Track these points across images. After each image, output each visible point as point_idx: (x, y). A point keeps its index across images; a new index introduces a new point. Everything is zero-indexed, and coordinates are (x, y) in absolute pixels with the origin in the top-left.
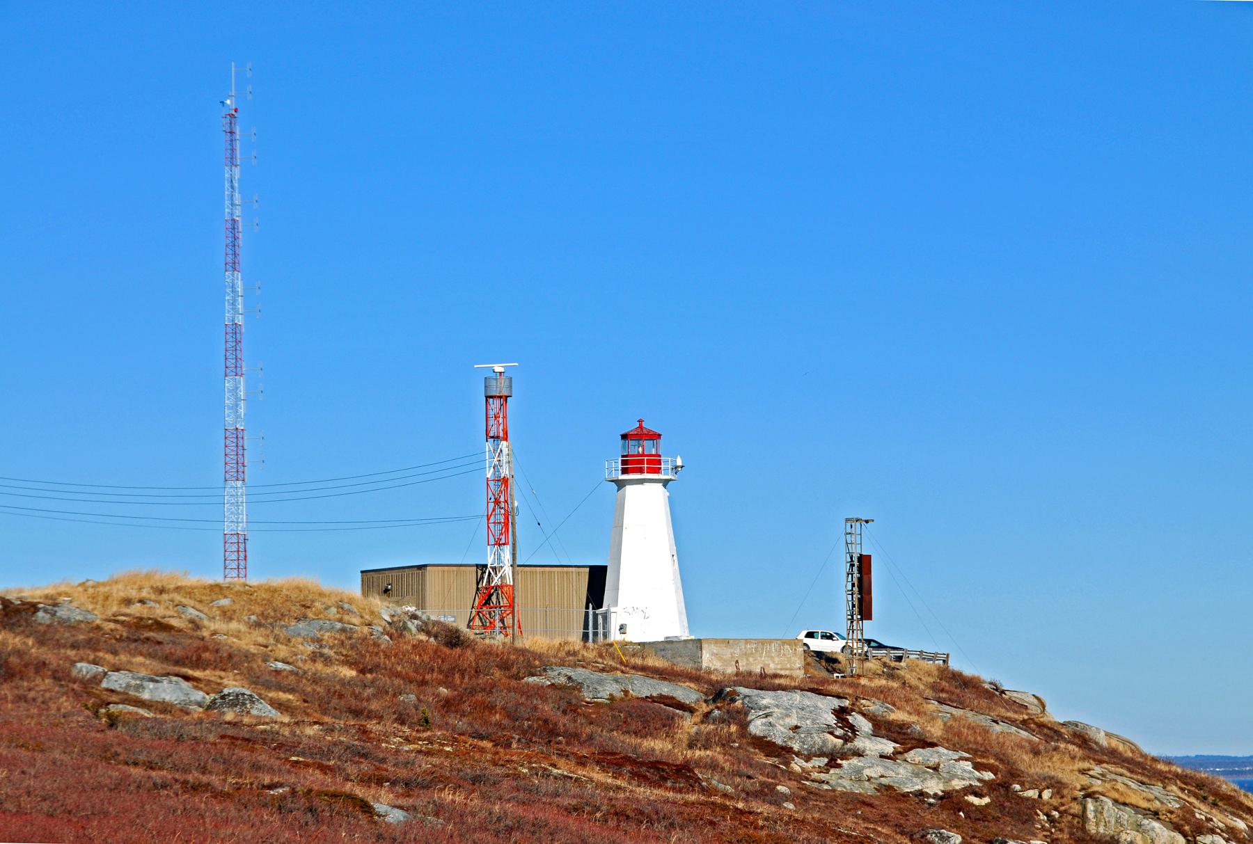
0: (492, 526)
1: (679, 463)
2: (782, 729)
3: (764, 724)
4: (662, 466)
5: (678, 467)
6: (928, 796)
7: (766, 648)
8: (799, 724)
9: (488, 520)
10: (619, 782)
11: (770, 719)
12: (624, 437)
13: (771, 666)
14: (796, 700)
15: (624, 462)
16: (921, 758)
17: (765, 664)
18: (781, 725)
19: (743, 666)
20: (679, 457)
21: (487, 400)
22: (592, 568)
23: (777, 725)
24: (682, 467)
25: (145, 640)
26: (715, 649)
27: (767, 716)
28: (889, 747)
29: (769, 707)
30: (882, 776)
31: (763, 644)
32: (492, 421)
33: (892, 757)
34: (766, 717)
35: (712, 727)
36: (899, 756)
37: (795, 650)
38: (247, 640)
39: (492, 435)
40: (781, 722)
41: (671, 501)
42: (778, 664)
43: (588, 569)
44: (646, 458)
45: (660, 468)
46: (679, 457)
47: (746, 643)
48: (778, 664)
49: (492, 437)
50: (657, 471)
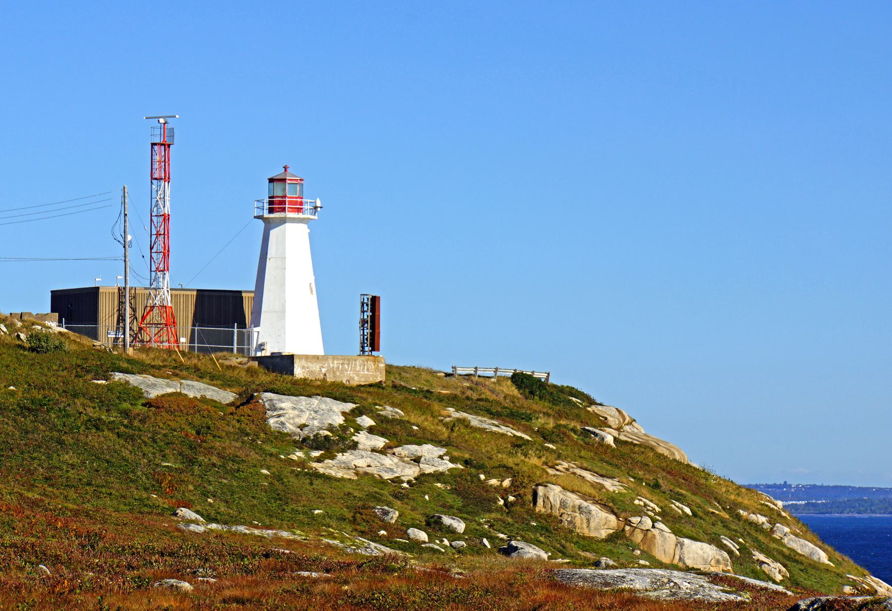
0: (154, 255)
1: (319, 204)
2: (291, 427)
3: (277, 422)
4: (287, 206)
5: (318, 207)
6: (403, 482)
7: (352, 364)
8: (307, 424)
9: (151, 248)
10: (656, 594)
11: (282, 419)
12: (271, 180)
13: (355, 378)
14: (313, 404)
15: (271, 203)
16: (406, 452)
17: (351, 377)
18: (290, 424)
19: (330, 378)
20: (318, 199)
21: (152, 148)
22: (198, 291)
23: (286, 423)
24: (321, 207)
25: (322, 459)
26: (303, 362)
27: (279, 416)
28: (380, 442)
29: (284, 409)
30: (369, 466)
31: (349, 360)
32: (156, 166)
33: (383, 451)
34: (279, 417)
35: (728, 517)
36: (390, 451)
37: (378, 366)
38: (155, 405)
39: (156, 177)
40: (291, 421)
41: (310, 235)
42: (362, 377)
43: (195, 293)
44: (287, 199)
45: (285, 208)
46: (318, 199)
47: (334, 359)
48: (362, 377)
49: (156, 179)
50: (299, 210)
